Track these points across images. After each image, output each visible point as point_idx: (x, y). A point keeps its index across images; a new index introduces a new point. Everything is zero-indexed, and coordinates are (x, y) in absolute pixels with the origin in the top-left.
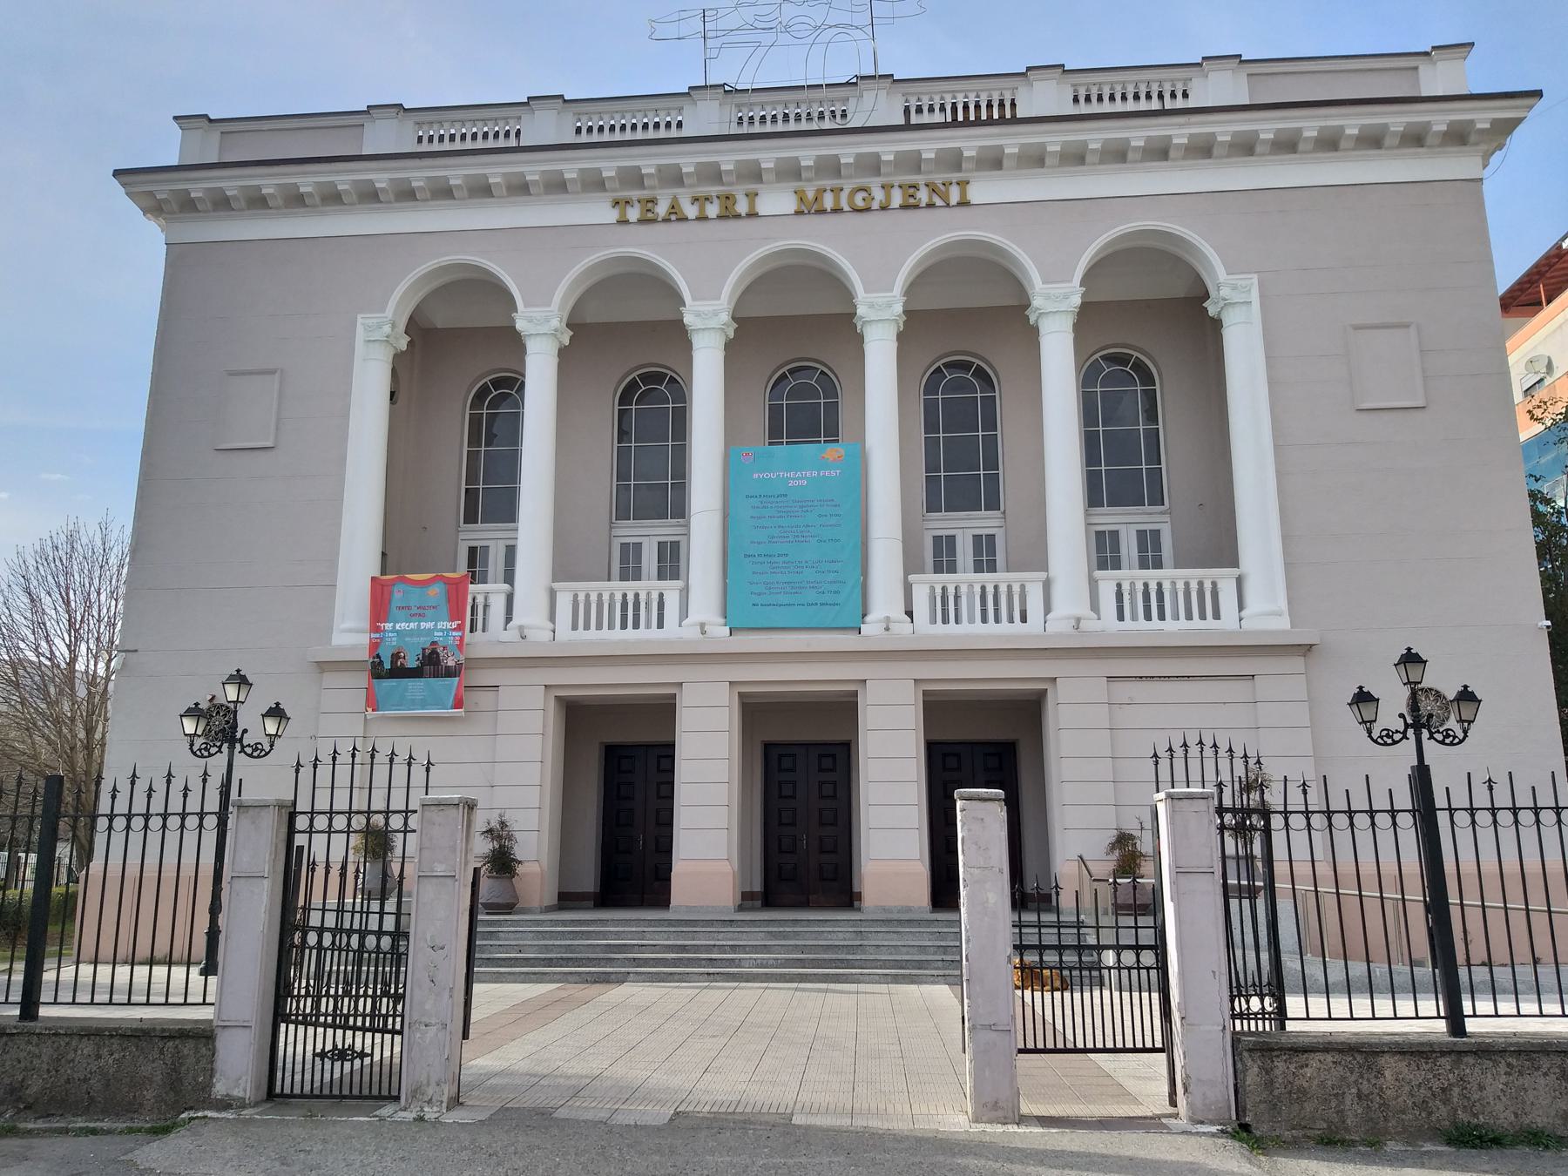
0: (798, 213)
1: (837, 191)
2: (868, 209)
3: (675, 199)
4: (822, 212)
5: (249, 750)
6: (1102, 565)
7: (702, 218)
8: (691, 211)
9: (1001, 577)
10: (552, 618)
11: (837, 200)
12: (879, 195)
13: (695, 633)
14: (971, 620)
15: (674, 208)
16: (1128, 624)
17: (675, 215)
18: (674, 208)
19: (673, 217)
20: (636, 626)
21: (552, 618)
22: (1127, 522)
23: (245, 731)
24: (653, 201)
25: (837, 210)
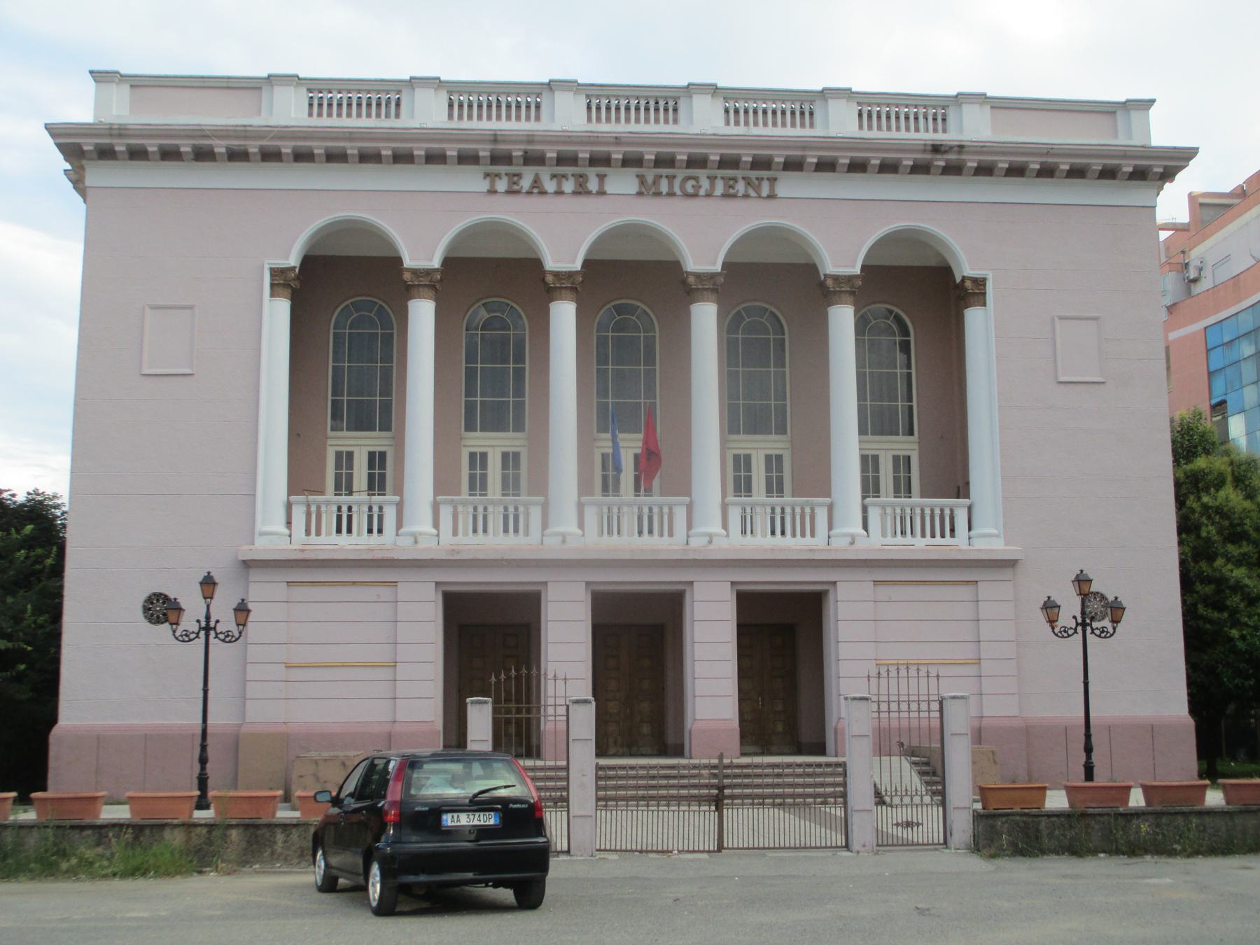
0: (640, 194)
1: (671, 178)
2: (695, 195)
3: (537, 176)
4: (658, 194)
5: (222, 636)
6: (737, 490)
7: (559, 193)
8: (550, 186)
9: (656, 499)
10: (289, 523)
11: (671, 185)
12: (705, 184)
13: (408, 541)
14: (329, 534)
15: (536, 182)
16: (323, 538)
17: (537, 188)
18: (536, 182)
19: (535, 191)
20: (318, 533)
21: (289, 523)
22: (759, 448)
23: (217, 621)
24: (519, 175)
25: (671, 194)
